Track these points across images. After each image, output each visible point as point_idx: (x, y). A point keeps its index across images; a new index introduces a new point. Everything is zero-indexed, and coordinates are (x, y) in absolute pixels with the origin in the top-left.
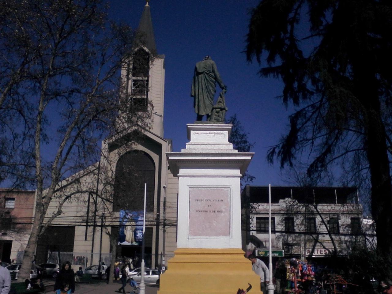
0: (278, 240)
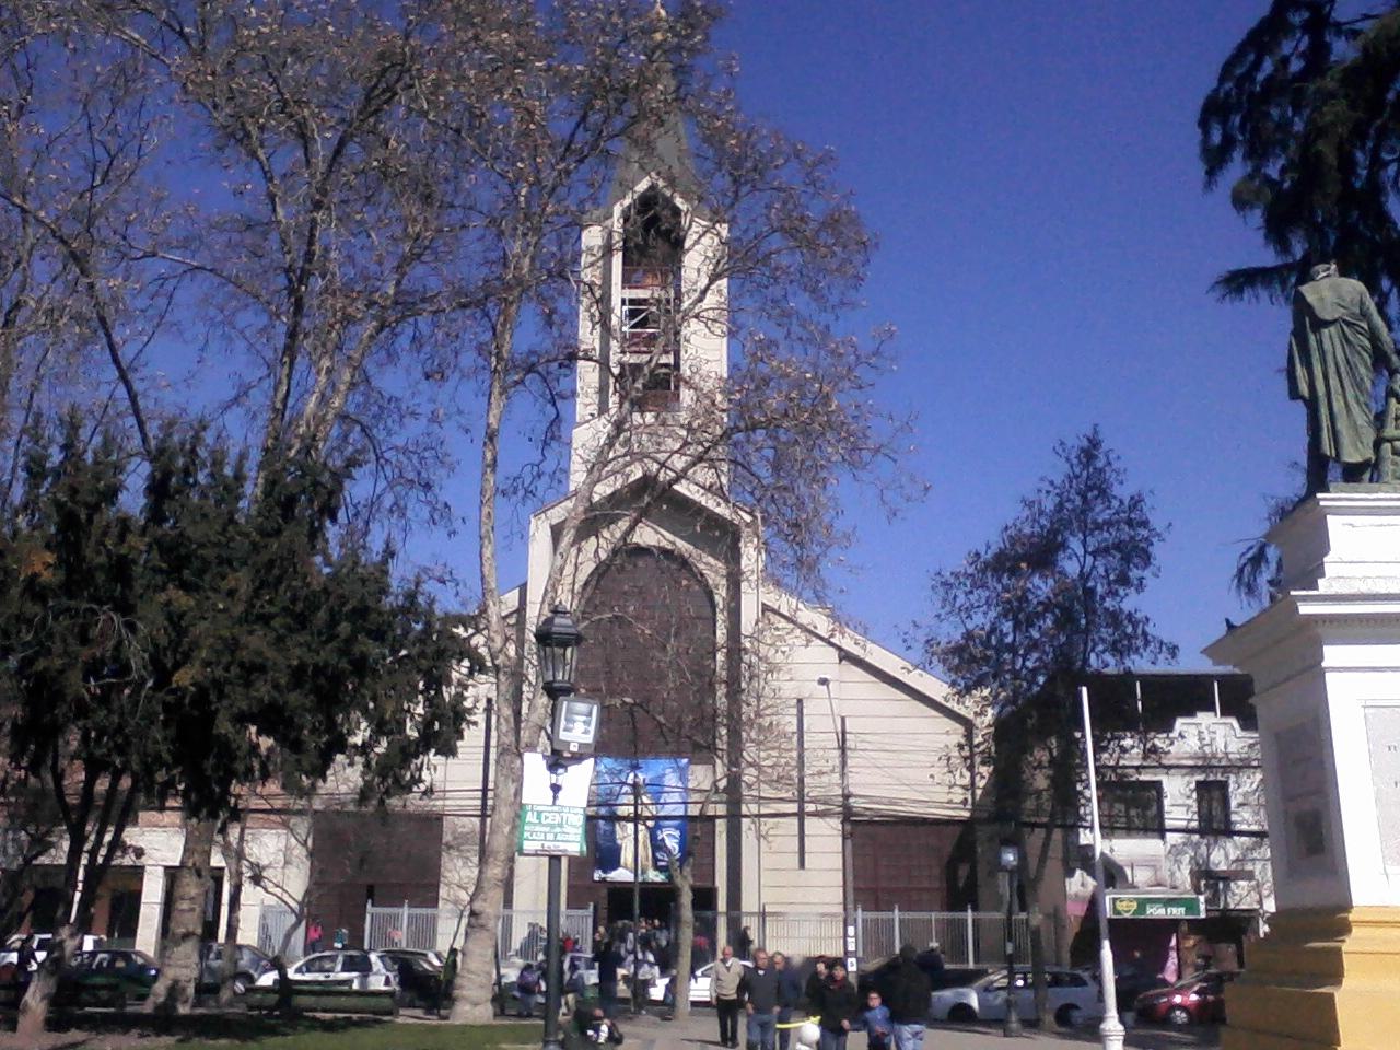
0: (1176, 861)
